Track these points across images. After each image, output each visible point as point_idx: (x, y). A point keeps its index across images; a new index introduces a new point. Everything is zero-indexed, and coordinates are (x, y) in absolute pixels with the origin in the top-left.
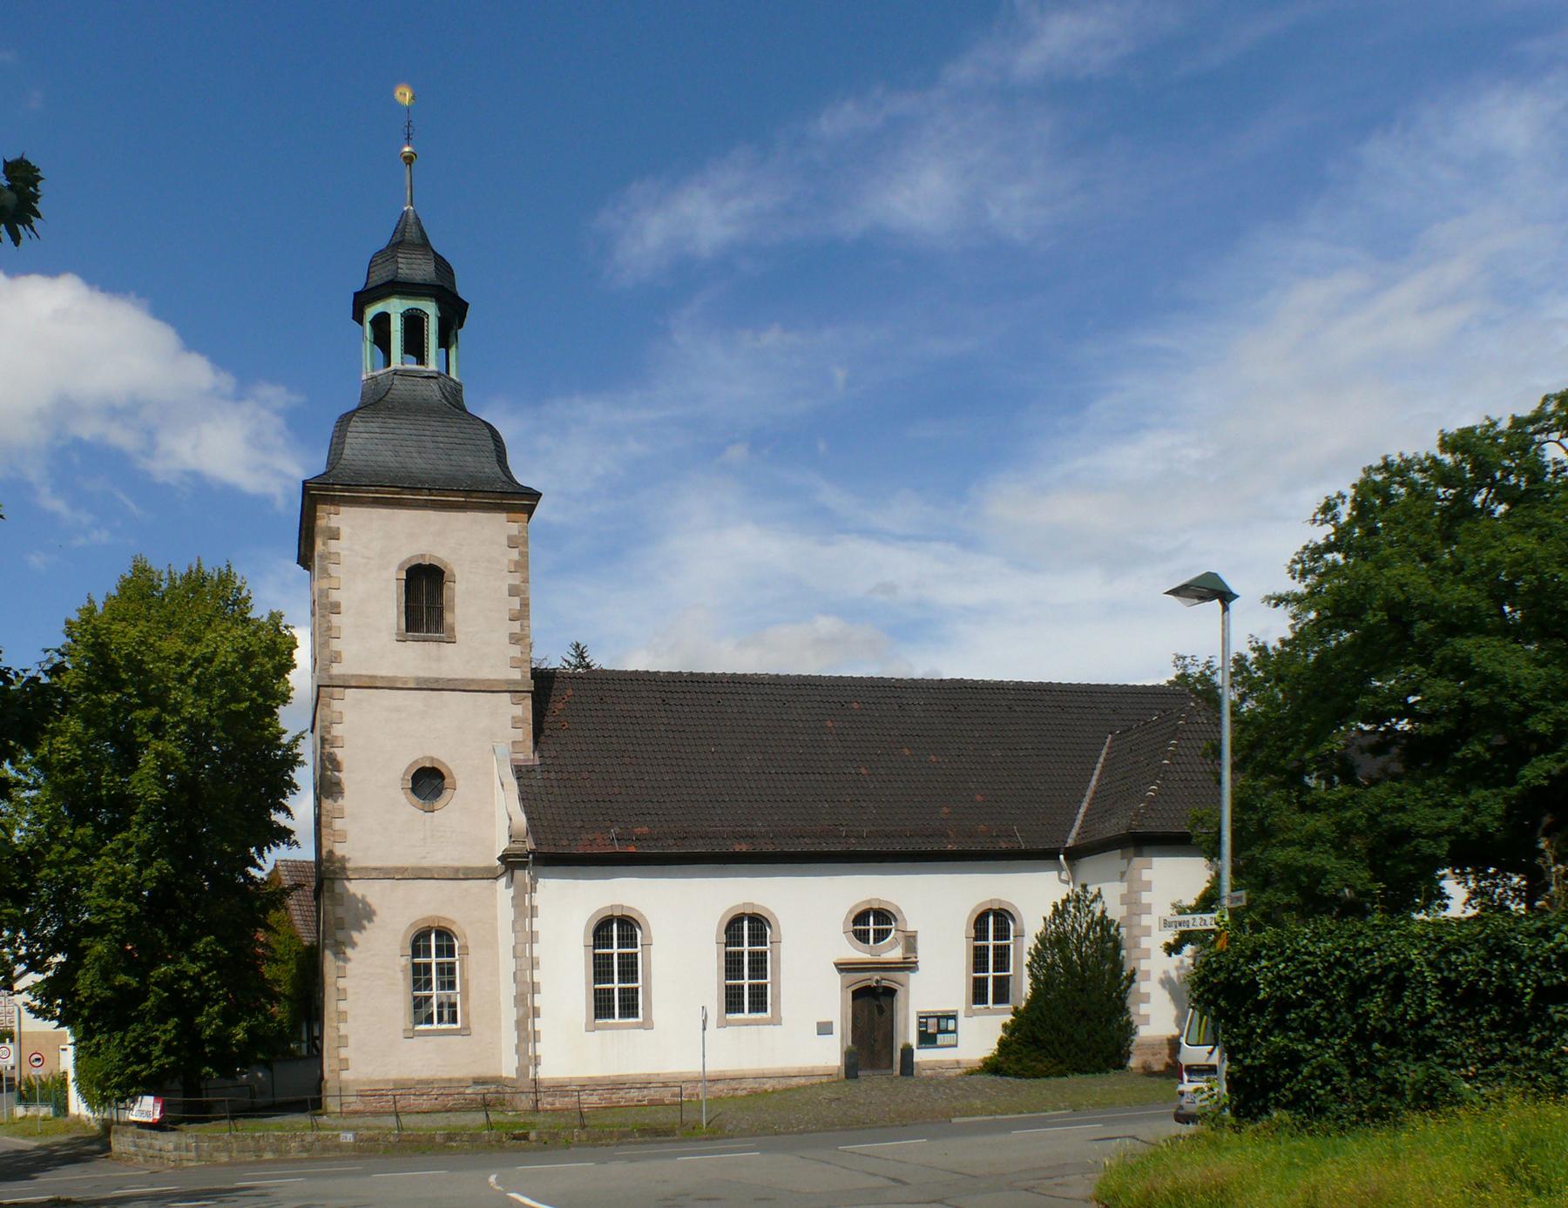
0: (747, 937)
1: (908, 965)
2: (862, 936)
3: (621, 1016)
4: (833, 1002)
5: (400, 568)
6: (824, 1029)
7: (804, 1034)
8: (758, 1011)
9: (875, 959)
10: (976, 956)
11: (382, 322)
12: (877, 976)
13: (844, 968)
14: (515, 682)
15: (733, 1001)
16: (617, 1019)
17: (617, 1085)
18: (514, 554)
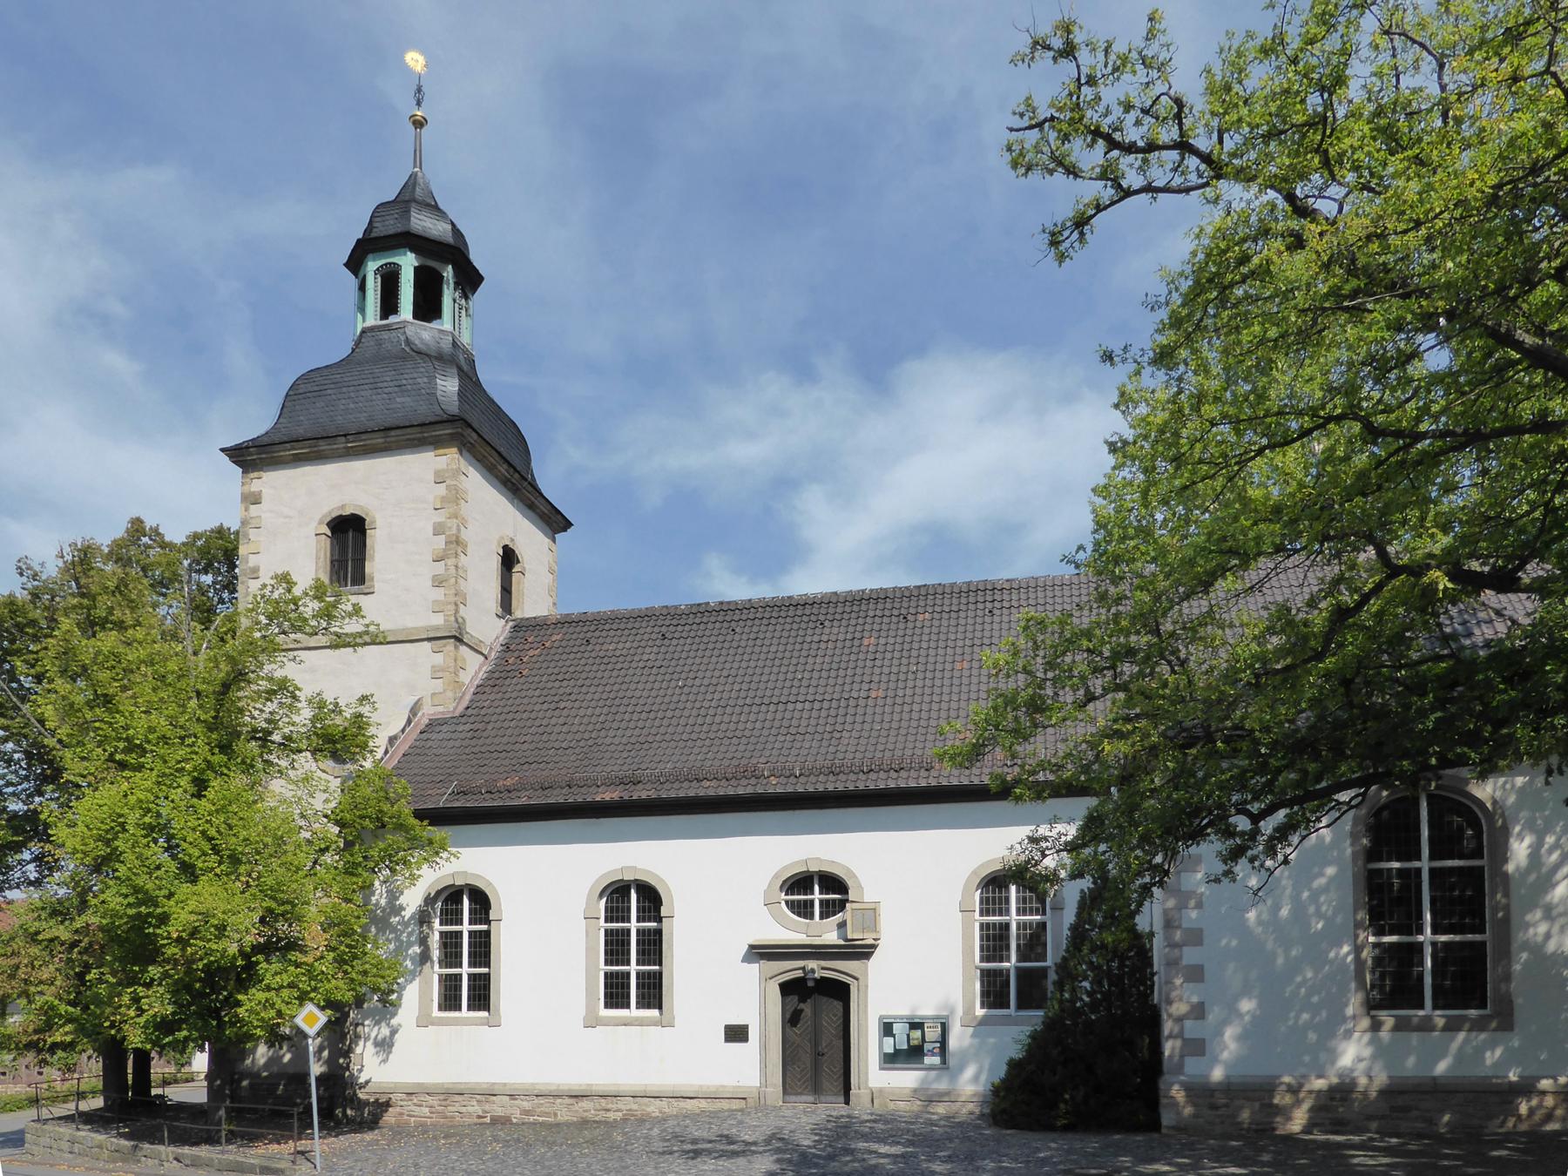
0: (634, 912)
1: (863, 952)
2: (804, 910)
3: (469, 1009)
4: (752, 997)
5: (320, 523)
6: (736, 1034)
7: (708, 1043)
8: (617, 1007)
9: (808, 941)
10: (487, 954)
11: (390, 280)
12: (812, 964)
13: (761, 953)
14: (437, 628)
15: (616, 993)
16: (465, 1012)
17: (450, 1094)
18: (441, 490)
